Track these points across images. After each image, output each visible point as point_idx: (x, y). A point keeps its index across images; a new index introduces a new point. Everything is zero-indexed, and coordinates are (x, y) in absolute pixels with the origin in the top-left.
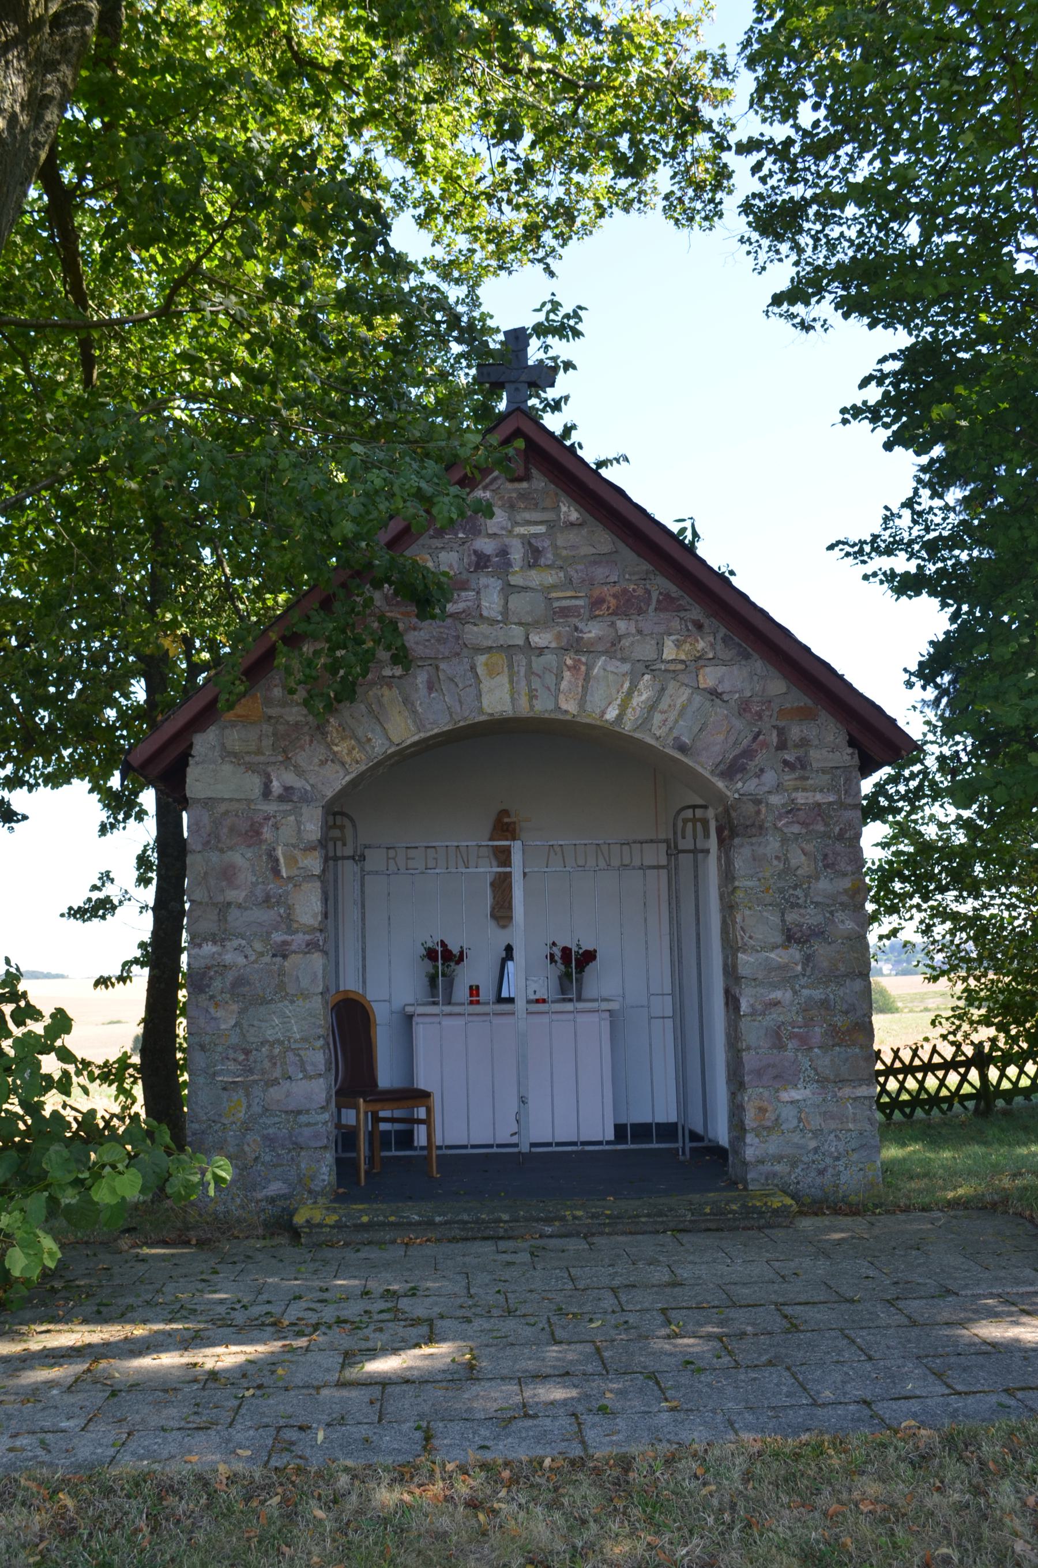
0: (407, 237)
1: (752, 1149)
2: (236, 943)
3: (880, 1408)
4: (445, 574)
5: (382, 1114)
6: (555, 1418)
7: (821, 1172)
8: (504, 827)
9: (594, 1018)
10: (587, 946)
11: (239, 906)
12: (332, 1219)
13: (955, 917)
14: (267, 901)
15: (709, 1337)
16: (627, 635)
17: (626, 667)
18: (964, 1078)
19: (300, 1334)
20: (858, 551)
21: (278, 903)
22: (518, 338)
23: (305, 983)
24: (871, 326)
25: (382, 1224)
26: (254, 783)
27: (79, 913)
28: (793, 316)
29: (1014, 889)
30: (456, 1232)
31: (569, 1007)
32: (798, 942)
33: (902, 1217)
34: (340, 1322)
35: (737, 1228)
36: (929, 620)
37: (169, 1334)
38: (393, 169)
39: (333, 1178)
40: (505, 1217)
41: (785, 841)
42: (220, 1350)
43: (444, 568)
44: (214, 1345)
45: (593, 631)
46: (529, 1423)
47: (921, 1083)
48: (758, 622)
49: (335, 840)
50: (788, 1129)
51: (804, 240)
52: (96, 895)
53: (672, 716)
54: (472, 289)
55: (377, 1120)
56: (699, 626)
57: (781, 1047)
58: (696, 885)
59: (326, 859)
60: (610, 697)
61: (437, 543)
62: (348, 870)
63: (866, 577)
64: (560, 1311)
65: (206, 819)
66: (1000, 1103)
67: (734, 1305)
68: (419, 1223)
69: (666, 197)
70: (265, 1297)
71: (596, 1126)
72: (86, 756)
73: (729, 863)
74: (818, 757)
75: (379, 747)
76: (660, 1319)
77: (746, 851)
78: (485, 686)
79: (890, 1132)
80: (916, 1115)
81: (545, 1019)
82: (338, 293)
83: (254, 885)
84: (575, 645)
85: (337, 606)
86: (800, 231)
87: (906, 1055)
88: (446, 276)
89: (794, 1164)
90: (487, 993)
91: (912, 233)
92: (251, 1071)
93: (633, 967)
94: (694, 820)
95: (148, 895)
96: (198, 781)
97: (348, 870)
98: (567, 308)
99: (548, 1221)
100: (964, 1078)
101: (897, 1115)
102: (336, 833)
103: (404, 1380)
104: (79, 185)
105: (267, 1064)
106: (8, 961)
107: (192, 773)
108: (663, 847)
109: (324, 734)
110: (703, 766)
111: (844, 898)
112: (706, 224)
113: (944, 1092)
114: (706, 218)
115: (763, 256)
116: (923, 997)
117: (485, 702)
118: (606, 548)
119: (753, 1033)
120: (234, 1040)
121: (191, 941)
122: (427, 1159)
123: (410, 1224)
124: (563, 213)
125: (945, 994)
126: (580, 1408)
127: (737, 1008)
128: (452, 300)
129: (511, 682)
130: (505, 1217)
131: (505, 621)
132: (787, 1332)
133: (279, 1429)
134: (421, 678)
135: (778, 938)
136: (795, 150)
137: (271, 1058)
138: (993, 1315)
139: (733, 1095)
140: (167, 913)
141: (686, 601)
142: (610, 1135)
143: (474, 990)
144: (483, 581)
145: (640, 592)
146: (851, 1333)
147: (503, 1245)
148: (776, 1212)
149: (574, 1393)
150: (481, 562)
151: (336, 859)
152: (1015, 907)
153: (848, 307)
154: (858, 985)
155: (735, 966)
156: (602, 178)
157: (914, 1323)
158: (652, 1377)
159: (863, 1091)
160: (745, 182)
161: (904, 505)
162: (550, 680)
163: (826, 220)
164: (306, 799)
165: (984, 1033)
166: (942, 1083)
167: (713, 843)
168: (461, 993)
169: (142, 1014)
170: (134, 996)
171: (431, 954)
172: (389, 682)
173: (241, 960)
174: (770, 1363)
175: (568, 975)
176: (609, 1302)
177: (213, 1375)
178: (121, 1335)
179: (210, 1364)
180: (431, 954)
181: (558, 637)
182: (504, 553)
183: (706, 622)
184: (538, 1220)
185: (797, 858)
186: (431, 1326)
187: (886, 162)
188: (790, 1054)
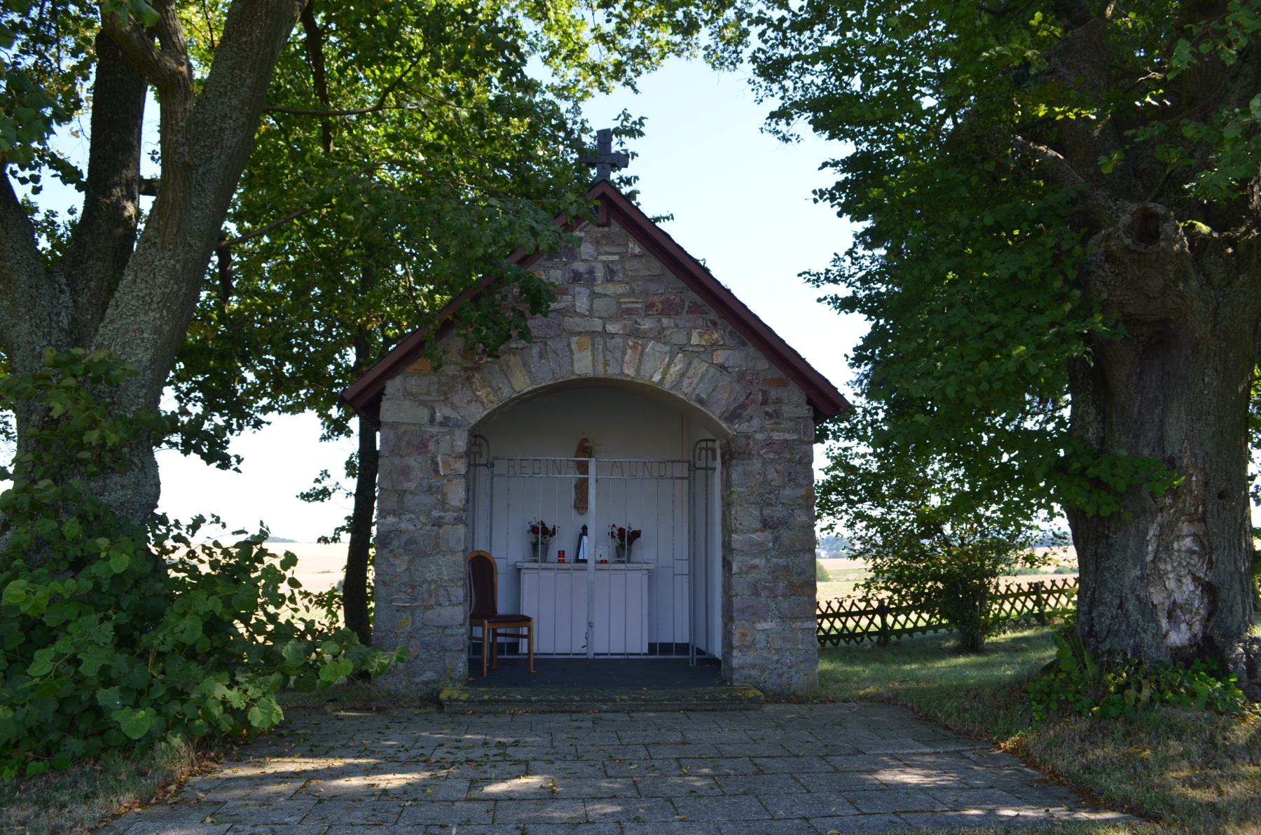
0: (535, 69)
1: (737, 659)
2: (409, 516)
3: (814, 822)
4: (552, 284)
5: (499, 631)
6: (606, 824)
7: (780, 676)
8: (585, 449)
9: (638, 574)
10: (635, 528)
11: (412, 493)
12: (464, 697)
13: (869, 518)
14: (430, 490)
15: (706, 776)
16: (668, 328)
17: (667, 348)
18: (871, 621)
19: (442, 768)
20: (816, 279)
21: (437, 492)
22: (605, 136)
23: (452, 544)
24: (831, 138)
25: (497, 701)
26: (424, 413)
27: (306, 497)
28: (778, 132)
29: (907, 503)
30: (545, 707)
31: (622, 566)
32: (771, 528)
33: (831, 705)
34: (468, 761)
35: (725, 710)
36: (859, 326)
37: (357, 766)
38: (528, 25)
39: (466, 671)
40: (577, 698)
41: (764, 463)
42: (390, 776)
43: (552, 280)
44: (386, 773)
45: (647, 324)
46: (590, 827)
47: (844, 624)
48: (752, 323)
49: (475, 453)
50: (760, 646)
51: (788, 84)
52: (319, 487)
53: (695, 381)
54: (576, 104)
55: (496, 635)
56: (715, 324)
57: (758, 595)
58: (707, 490)
59: (469, 465)
60: (656, 367)
61: (549, 264)
62: (483, 473)
63: (819, 300)
64: (611, 758)
65: (392, 436)
66: (893, 638)
67: (722, 757)
68: (521, 701)
69: (706, 48)
70: (420, 744)
71: (637, 644)
72: (314, 396)
73: (728, 476)
74: (787, 410)
75: (506, 393)
76: (675, 764)
77: (740, 469)
78: (576, 357)
79: (824, 653)
80: (843, 645)
81: (607, 574)
82: (490, 101)
83: (422, 479)
84: (635, 333)
85: (484, 302)
86: (785, 77)
87: (835, 606)
88: (559, 96)
89: (763, 670)
90: (569, 556)
91: (856, 83)
92: (415, 599)
93: (664, 543)
94: (707, 449)
95: (352, 484)
96: (387, 411)
97: (483, 473)
98: (635, 118)
99: (604, 701)
100: (871, 621)
101: (828, 644)
102: (476, 449)
103: (509, 797)
104: (326, 27)
105: (426, 596)
106: (262, 523)
107: (385, 406)
108: (686, 465)
109: (471, 384)
110: (714, 413)
111: (801, 501)
112: (731, 67)
113: (858, 630)
114: (732, 63)
115: (761, 92)
116: (845, 572)
117: (576, 366)
118: (657, 272)
119: (740, 585)
120: (406, 579)
121: (379, 516)
122: (527, 661)
123: (516, 701)
124: (639, 53)
125: (862, 568)
126: (622, 818)
127: (730, 569)
128: (563, 110)
129: (593, 355)
130: (577, 698)
131: (591, 316)
132: (757, 774)
133: (427, 826)
134: (535, 350)
135: (758, 525)
136: (786, 25)
137: (429, 591)
138: (888, 767)
139: (725, 625)
140: (363, 498)
141: (707, 307)
142: (646, 650)
143: (561, 554)
144: (578, 289)
145: (678, 301)
146: (798, 776)
147: (574, 716)
148: (751, 700)
149: (619, 809)
150: (576, 277)
151: (475, 465)
152: (907, 514)
153: (818, 126)
154: (808, 557)
155: (730, 542)
156: (665, 35)
157: (837, 771)
158: (669, 799)
159: (808, 625)
160: (754, 42)
161: (847, 253)
162: (618, 354)
163: (803, 71)
164: (457, 425)
165: (885, 594)
166: (857, 624)
167: (718, 464)
168: (553, 555)
169: (345, 563)
170: (341, 551)
171: (534, 530)
172: (514, 351)
173: (412, 528)
174: (745, 793)
175: (622, 546)
176: (642, 753)
177: (385, 792)
178: (326, 765)
179: (383, 785)
180: (534, 530)
181: (624, 327)
182: (591, 272)
183: (719, 322)
184: (598, 701)
185: (772, 474)
186: (527, 765)
187: (844, 35)
188: (763, 600)
